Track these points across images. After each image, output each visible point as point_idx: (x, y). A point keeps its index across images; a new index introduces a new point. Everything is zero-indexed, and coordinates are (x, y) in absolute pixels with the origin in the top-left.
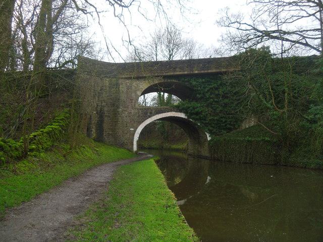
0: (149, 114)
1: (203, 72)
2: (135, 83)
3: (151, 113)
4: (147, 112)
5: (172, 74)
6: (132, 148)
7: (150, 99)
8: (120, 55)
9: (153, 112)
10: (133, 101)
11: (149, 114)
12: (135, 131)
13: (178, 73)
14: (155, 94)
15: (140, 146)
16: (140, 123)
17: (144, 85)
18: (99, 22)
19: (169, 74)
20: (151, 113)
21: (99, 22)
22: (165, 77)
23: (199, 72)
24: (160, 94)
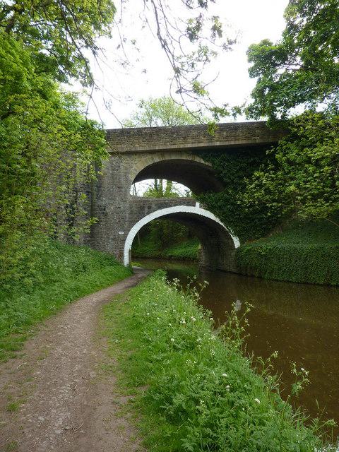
0: (146, 209)
1: (227, 143)
2: (125, 162)
3: (149, 208)
4: (143, 206)
5: (182, 146)
6: (122, 262)
7: (143, 188)
8: (111, 124)
9: (153, 206)
10: (123, 190)
11: (146, 209)
12: (125, 236)
13: (189, 146)
14: (151, 181)
15: (134, 256)
16: (133, 223)
17: (139, 165)
18: (158, 34)
19: (175, 147)
20: (149, 208)
21: (158, 34)
22: (162, 152)
23: (222, 144)
24: (156, 182)
